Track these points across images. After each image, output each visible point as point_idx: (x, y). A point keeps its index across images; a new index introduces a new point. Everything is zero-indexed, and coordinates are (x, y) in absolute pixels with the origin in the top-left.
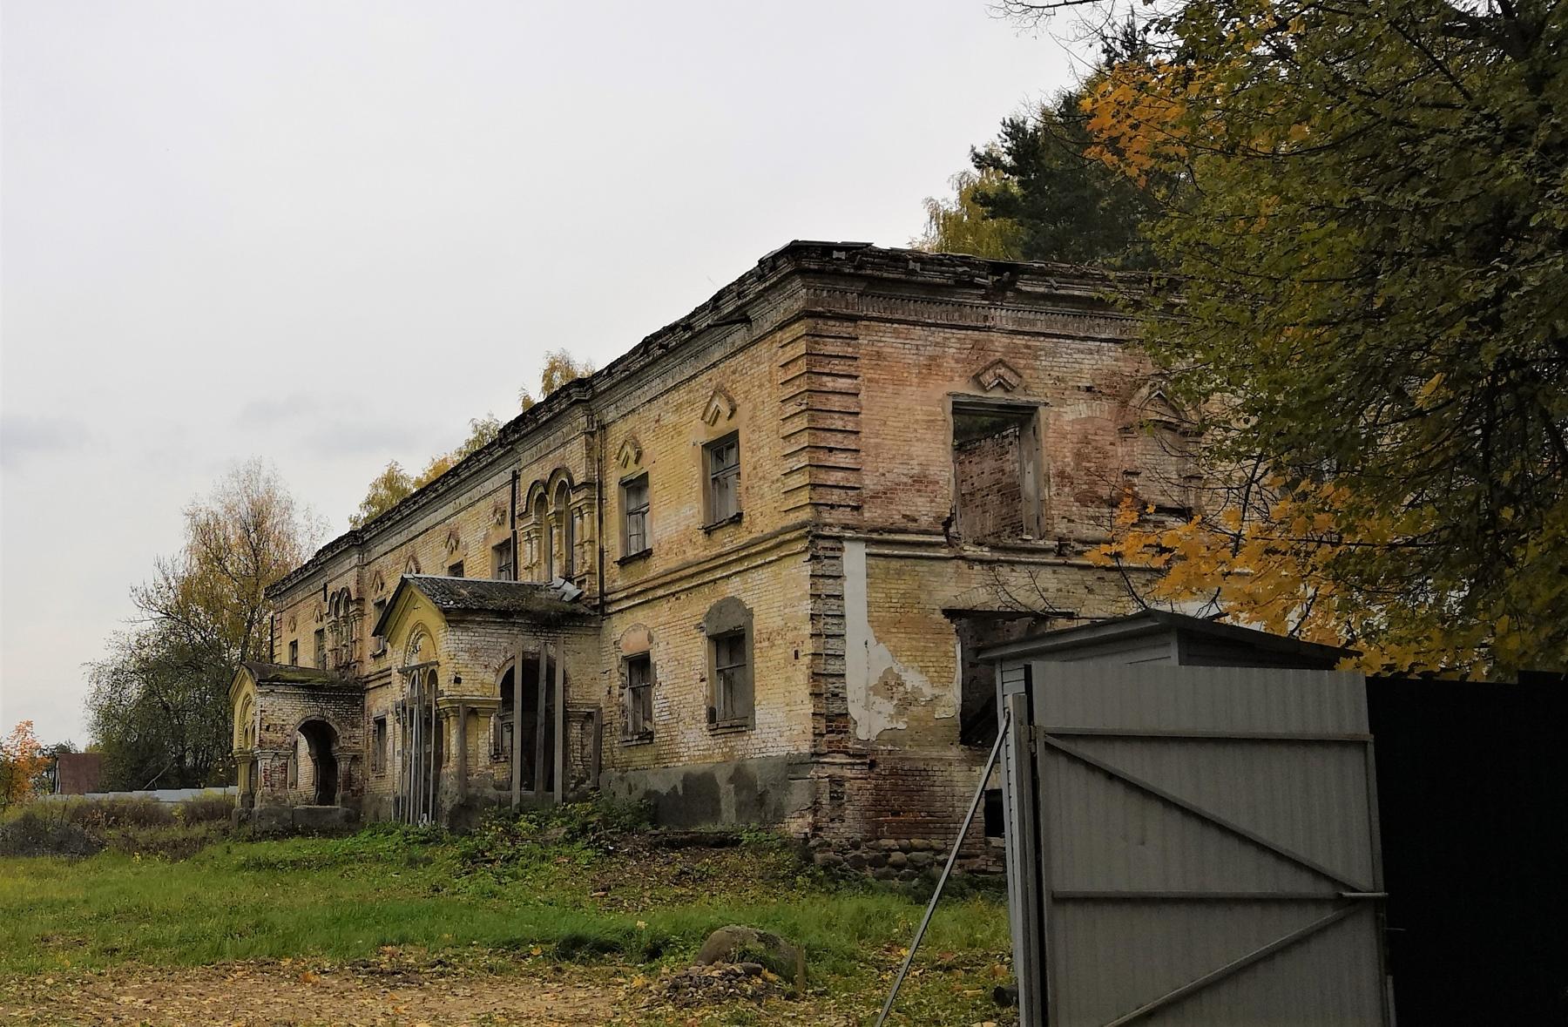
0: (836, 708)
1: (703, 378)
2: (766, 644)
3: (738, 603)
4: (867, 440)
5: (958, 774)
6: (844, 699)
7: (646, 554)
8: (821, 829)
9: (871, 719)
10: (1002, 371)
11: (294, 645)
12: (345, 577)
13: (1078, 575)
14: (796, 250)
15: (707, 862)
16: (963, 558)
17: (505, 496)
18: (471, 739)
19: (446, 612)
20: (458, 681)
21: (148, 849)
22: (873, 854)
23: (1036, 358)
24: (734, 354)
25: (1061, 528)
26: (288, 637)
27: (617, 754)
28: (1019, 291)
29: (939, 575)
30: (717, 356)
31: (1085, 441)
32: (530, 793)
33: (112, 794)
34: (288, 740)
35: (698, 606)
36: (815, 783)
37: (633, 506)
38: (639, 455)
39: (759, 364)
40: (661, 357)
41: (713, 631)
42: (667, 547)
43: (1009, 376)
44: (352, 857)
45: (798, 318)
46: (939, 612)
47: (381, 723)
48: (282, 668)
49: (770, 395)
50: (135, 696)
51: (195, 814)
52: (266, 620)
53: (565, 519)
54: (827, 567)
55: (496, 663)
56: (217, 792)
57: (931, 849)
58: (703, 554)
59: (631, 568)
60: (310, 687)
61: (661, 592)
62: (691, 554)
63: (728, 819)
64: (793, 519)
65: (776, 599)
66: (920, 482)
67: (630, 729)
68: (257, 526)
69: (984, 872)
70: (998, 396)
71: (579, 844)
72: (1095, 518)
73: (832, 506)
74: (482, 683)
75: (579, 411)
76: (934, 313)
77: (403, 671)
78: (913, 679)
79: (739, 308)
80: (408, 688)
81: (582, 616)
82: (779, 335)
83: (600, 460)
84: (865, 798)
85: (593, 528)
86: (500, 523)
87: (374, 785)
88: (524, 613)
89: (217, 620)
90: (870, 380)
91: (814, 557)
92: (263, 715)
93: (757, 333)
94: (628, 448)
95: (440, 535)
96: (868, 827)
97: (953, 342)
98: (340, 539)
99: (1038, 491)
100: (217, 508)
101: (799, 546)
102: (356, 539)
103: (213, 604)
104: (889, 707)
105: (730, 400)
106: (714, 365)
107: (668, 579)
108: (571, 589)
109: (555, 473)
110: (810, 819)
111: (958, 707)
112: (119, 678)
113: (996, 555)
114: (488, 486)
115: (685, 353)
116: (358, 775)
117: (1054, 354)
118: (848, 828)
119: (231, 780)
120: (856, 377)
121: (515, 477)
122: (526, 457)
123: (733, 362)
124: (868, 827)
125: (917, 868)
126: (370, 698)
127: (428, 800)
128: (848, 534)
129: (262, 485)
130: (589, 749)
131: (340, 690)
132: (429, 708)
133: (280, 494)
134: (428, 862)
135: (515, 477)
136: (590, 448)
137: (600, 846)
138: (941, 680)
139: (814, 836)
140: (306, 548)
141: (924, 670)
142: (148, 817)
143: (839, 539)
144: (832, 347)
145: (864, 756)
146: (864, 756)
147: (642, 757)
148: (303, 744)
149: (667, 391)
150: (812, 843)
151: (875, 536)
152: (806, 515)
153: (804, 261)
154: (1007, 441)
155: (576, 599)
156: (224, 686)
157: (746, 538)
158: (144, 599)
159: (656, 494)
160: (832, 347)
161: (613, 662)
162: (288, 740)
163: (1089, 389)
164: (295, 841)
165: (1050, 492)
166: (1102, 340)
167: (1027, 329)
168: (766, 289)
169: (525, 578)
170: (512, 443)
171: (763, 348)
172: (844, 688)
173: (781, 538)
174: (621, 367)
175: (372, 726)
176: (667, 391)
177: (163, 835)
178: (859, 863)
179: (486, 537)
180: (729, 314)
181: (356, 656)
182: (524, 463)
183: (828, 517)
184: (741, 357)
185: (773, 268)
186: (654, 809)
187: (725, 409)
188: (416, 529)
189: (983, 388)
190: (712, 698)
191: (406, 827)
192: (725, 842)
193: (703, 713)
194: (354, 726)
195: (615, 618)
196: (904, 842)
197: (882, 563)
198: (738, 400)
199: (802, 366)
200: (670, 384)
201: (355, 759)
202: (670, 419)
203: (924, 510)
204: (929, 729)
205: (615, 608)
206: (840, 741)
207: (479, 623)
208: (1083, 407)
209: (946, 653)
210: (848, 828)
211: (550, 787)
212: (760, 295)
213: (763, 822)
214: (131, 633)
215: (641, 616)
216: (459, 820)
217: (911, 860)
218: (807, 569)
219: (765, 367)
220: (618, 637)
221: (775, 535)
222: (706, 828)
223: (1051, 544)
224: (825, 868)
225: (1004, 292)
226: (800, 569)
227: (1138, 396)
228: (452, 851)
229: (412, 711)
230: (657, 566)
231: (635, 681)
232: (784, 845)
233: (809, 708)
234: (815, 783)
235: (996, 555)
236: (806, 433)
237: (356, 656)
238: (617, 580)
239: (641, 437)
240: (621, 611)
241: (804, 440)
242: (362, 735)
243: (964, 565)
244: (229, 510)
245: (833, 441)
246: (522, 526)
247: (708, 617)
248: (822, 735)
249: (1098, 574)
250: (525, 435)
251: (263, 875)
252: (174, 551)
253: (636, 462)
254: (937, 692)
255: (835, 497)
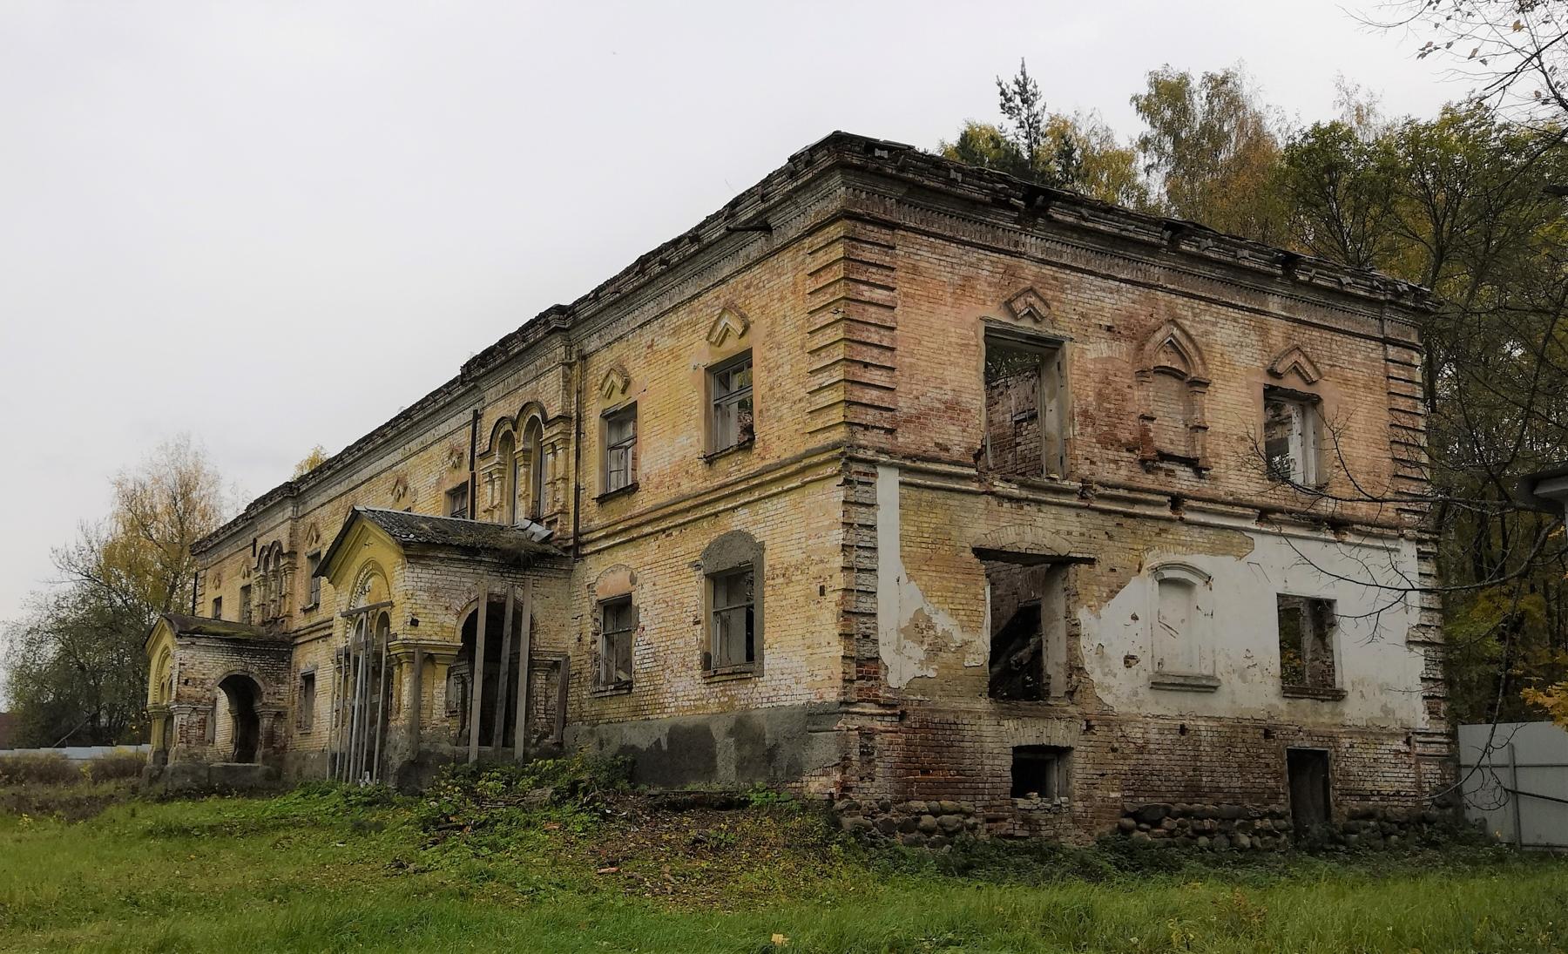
0: (867, 651)
1: (710, 295)
2: (781, 580)
3: (745, 537)
4: (902, 359)
5: (987, 728)
6: (875, 641)
7: (633, 489)
8: (850, 789)
9: (903, 668)
10: (1032, 299)
11: (218, 602)
12: (278, 530)
13: (1099, 520)
14: (838, 141)
15: (720, 827)
16: (993, 494)
17: (464, 438)
18: (426, 689)
19: (406, 545)
20: (415, 623)
21: (45, 808)
22: (904, 817)
23: (1063, 291)
24: (748, 267)
25: (1084, 469)
26: (211, 594)
27: (586, 706)
28: (1050, 219)
29: (970, 510)
30: (726, 272)
31: (1106, 381)
32: (489, 749)
33: (17, 752)
34: (208, 694)
35: (695, 542)
36: (843, 736)
37: (614, 441)
38: (627, 383)
39: (779, 275)
40: (662, 274)
41: (711, 569)
42: (657, 480)
43: (1038, 305)
44: (282, 822)
45: (833, 220)
46: (969, 550)
47: (309, 679)
48: (204, 620)
49: (793, 308)
50: (50, 655)
51: (103, 772)
52: (189, 587)
53: (536, 458)
54: (860, 494)
55: (458, 605)
56: (129, 750)
57: (961, 812)
58: (700, 485)
59: (612, 505)
60: (234, 641)
61: (648, 529)
62: (686, 487)
63: (726, 777)
64: (821, 440)
65: (796, 533)
66: (953, 408)
67: (603, 678)
68: (185, 495)
69: (1011, 837)
70: (1027, 325)
71: (568, 808)
72: (1116, 462)
73: (866, 427)
74: (442, 627)
75: (557, 341)
76: (968, 232)
77: (348, 616)
78: (944, 622)
79: (760, 213)
80: (352, 633)
81: (551, 558)
82: (807, 241)
83: (579, 392)
84: (894, 756)
85: (567, 465)
86: (456, 467)
87: (298, 742)
88: (493, 550)
89: (140, 584)
90: (906, 295)
91: (847, 482)
92: (182, 669)
93: (778, 242)
94: (614, 377)
95: (388, 480)
96: (897, 786)
97: (986, 265)
98: (274, 491)
99: (1062, 429)
100: (145, 478)
101: (829, 470)
102: (291, 490)
103: (136, 569)
104: (919, 652)
105: (743, 316)
106: (723, 281)
107: (659, 513)
108: (540, 530)
109: (525, 408)
110: (837, 777)
111: (988, 655)
112: (33, 638)
113: (1024, 493)
114: (444, 429)
115: (687, 272)
116: (281, 732)
117: (1077, 288)
118: (878, 788)
119: (145, 739)
120: (893, 289)
121: (477, 416)
122: (490, 395)
123: (747, 276)
124: (897, 786)
125: (948, 834)
126: (298, 654)
127: (372, 757)
128: (883, 458)
129: (190, 458)
130: (554, 701)
131: (266, 646)
132: (378, 655)
133: (207, 468)
134: (379, 827)
135: (477, 416)
136: (567, 381)
137: (595, 809)
138: (970, 625)
139: (841, 797)
140: (230, 508)
141: (954, 613)
142: (55, 774)
143: (873, 463)
144: (870, 254)
145: (893, 706)
146: (893, 706)
147: (616, 708)
148: (223, 701)
149: (663, 314)
150: (839, 805)
151: (908, 463)
152: (839, 435)
153: (845, 156)
154: (996, 392)
155: (546, 540)
156: (142, 645)
157: (758, 465)
158: (65, 561)
159: (647, 424)
160: (870, 254)
161: (587, 607)
162: (208, 694)
163: (1109, 329)
164: (212, 801)
165: (1074, 431)
166: (1121, 281)
167: (1054, 259)
168: (796, 190)
169: (482, 518)
170: (476, 379)
171: (786, 257)
172: (876, 629)
173: (806, 462)
174: (612, 289)
175: (299, 682)
176: (663, 314)
177: (66, 793)
178: (889, 828)
179: (439, 482)
180: (746, 225)
181: (285, 610)
182: (487, 401)
183: (862, 438)
184: (756, 270)
185: (809, 163)
186: (631, 768)
187: (737, 326)
188: (357, 478)
189: (1014, 315)
190: (708, 642)
191: (344, 786)
192: (731, 803)
193: (697, 658)
194: (280, 681)
195: (589, 560)
196: (934, 804)
197: (913, 493)
198: (752, 316)
199: (839, 271)
200: (667, 305)
201: (279, 715)
202: (665, 343)
203: (956, 439)
204: (959, 678)
205: (590, 549)
206: (869, 689)
207: (442, 560)
208: (1104, 346)
209: (975, 596)
210: (878, 788)
211: (508, 741)
212: (788, 197)
213: (772, 781)
214: (49, 594)
215: (621, 556)
216: (402, 777)
217: (941, 825)
218: (841, 494)
219: (788, 278)
220: (593, 579)
221: (798, 459)
222: (696, 786)
223: (1076, 485)
224: (855, 834)
225: (1035, 218)
226: (831, 496)
227: (1153, 340)
228: (407, 815)
229: (356, 659)
230: (644, 501)
231: (609, 627)
232: (804, 808)
233: (838, 650)
234: (843, 736)
235: (1024, 493)
236: (842, 345)
237: (285, 610)
238: (595, 518)
239: (629, 366)
240: (598, 552)
241: (840, 352)
242: (288, 691)
243: (994, 502)
244: (157, 481)
245: (869, 355)
246: (482, 466)
247: (707, 554)
248: (852, 681)
249: (1117, 520)
250: (493, 370)
251: (175, 845)
252: (96, 517)
253: (623, 391)
254: (967, 637)
255: (870, 417)
